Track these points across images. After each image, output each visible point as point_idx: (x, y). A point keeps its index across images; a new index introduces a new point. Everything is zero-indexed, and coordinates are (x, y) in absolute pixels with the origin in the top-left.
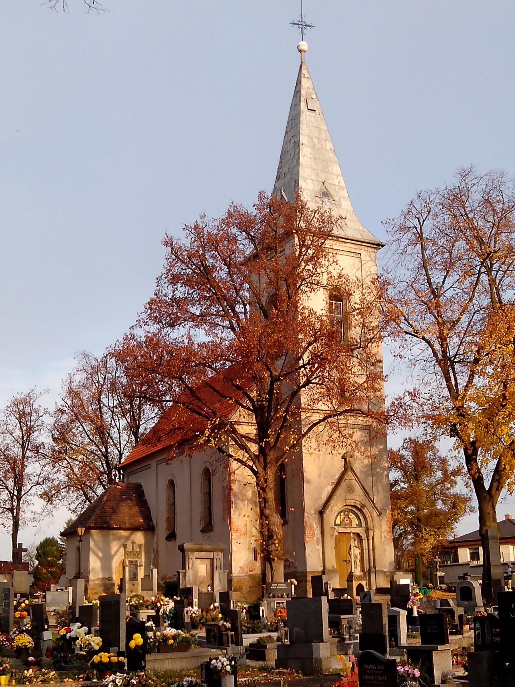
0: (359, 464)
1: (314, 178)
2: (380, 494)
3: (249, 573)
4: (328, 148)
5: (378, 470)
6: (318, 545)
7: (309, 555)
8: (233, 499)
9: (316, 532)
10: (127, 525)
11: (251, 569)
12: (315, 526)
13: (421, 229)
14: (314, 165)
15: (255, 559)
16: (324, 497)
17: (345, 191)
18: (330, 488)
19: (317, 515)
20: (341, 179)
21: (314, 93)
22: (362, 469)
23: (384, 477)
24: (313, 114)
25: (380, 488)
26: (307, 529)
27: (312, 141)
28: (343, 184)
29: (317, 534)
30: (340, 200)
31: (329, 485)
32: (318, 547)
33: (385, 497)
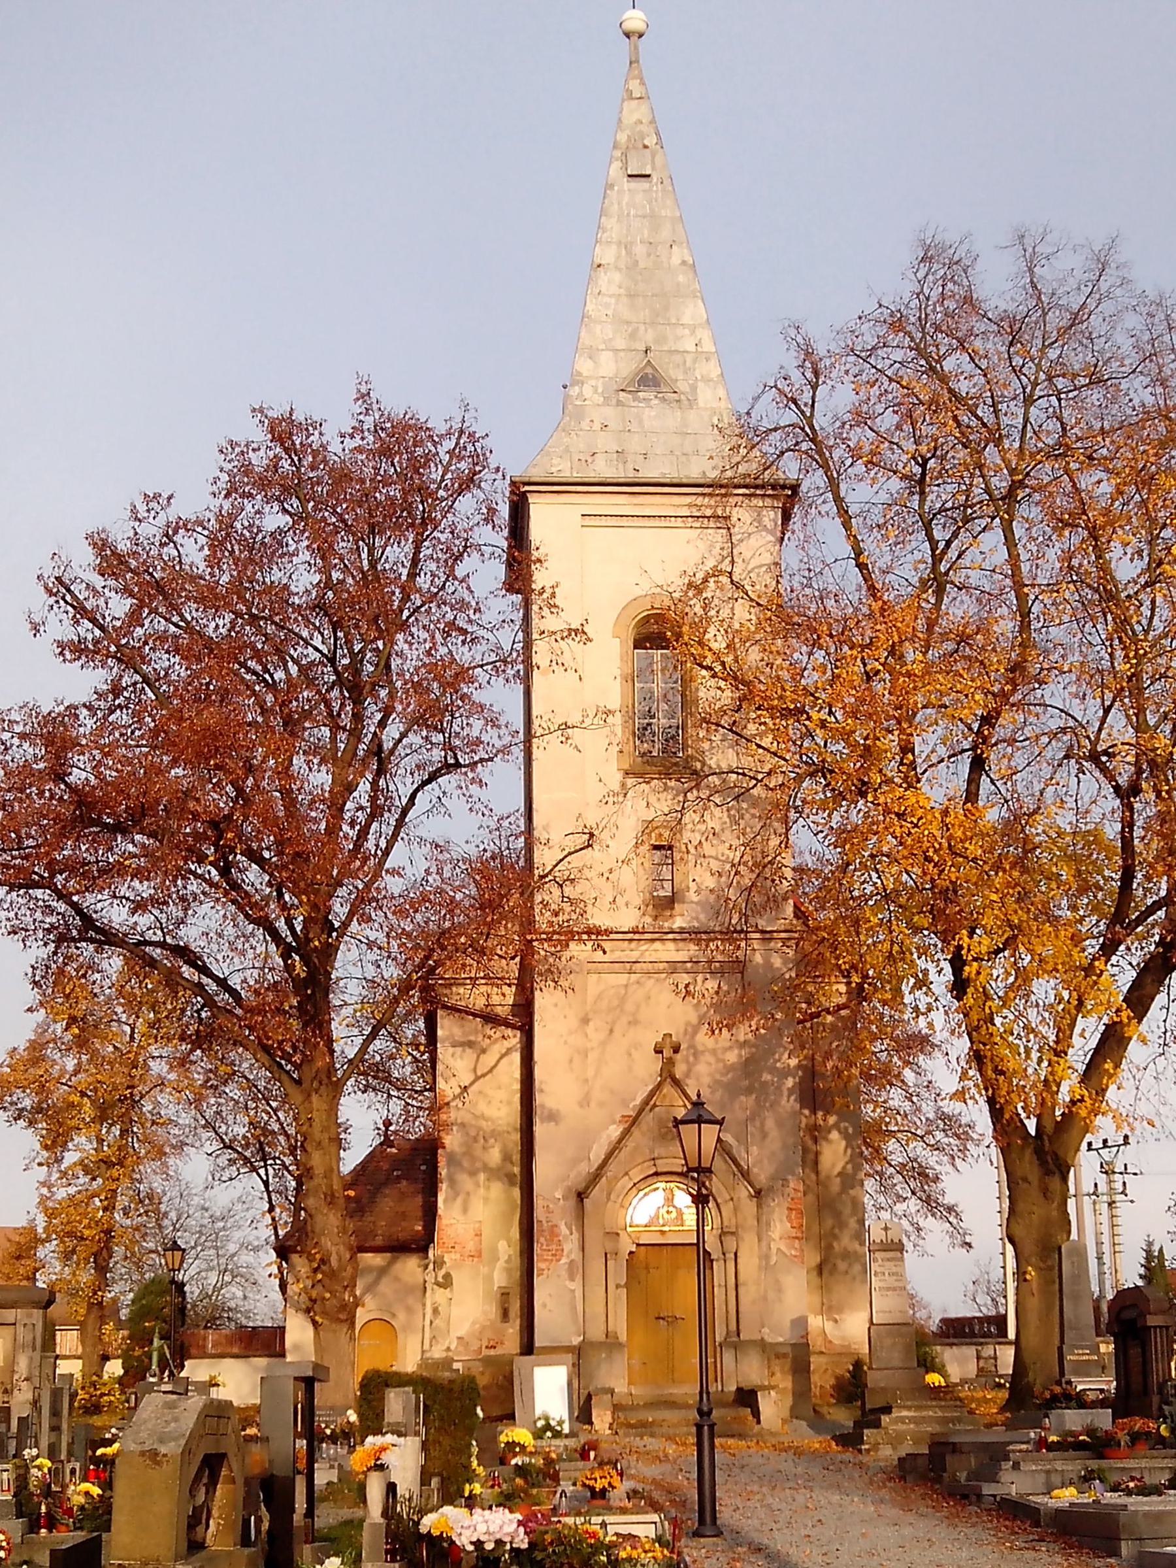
0: (709, 1064)
1: (620, 343)
2: (768, 1140)
3: (485, 1352)
4: (676, 260)
5: (766, 1077)
6: (572, 1279)
7: (544, 1305)
8: (443, 1171)
9: (567, 1247)
10: (379, 1241)
11: (492, 1343)
12: (564, 1230)
13: (812, 427)
14: (626, 314)
15: (505, 1315)
16: (597, 1154)
17: (713, 362)
18: (615, 1131)
19: (572, 1202)
20: (705, 335)
21: (652, 131)
22: (718, 1077)
23: (786, 1093)
24: (643, 184)
25: (770, 1123)
26: (542, 1240)
27: (629, 253)
28: (708, 346)
29: (571, 1252)
30: (694, 388)
31: (614, 1123)
32: (572, 1286)
33: (785, 1146)
